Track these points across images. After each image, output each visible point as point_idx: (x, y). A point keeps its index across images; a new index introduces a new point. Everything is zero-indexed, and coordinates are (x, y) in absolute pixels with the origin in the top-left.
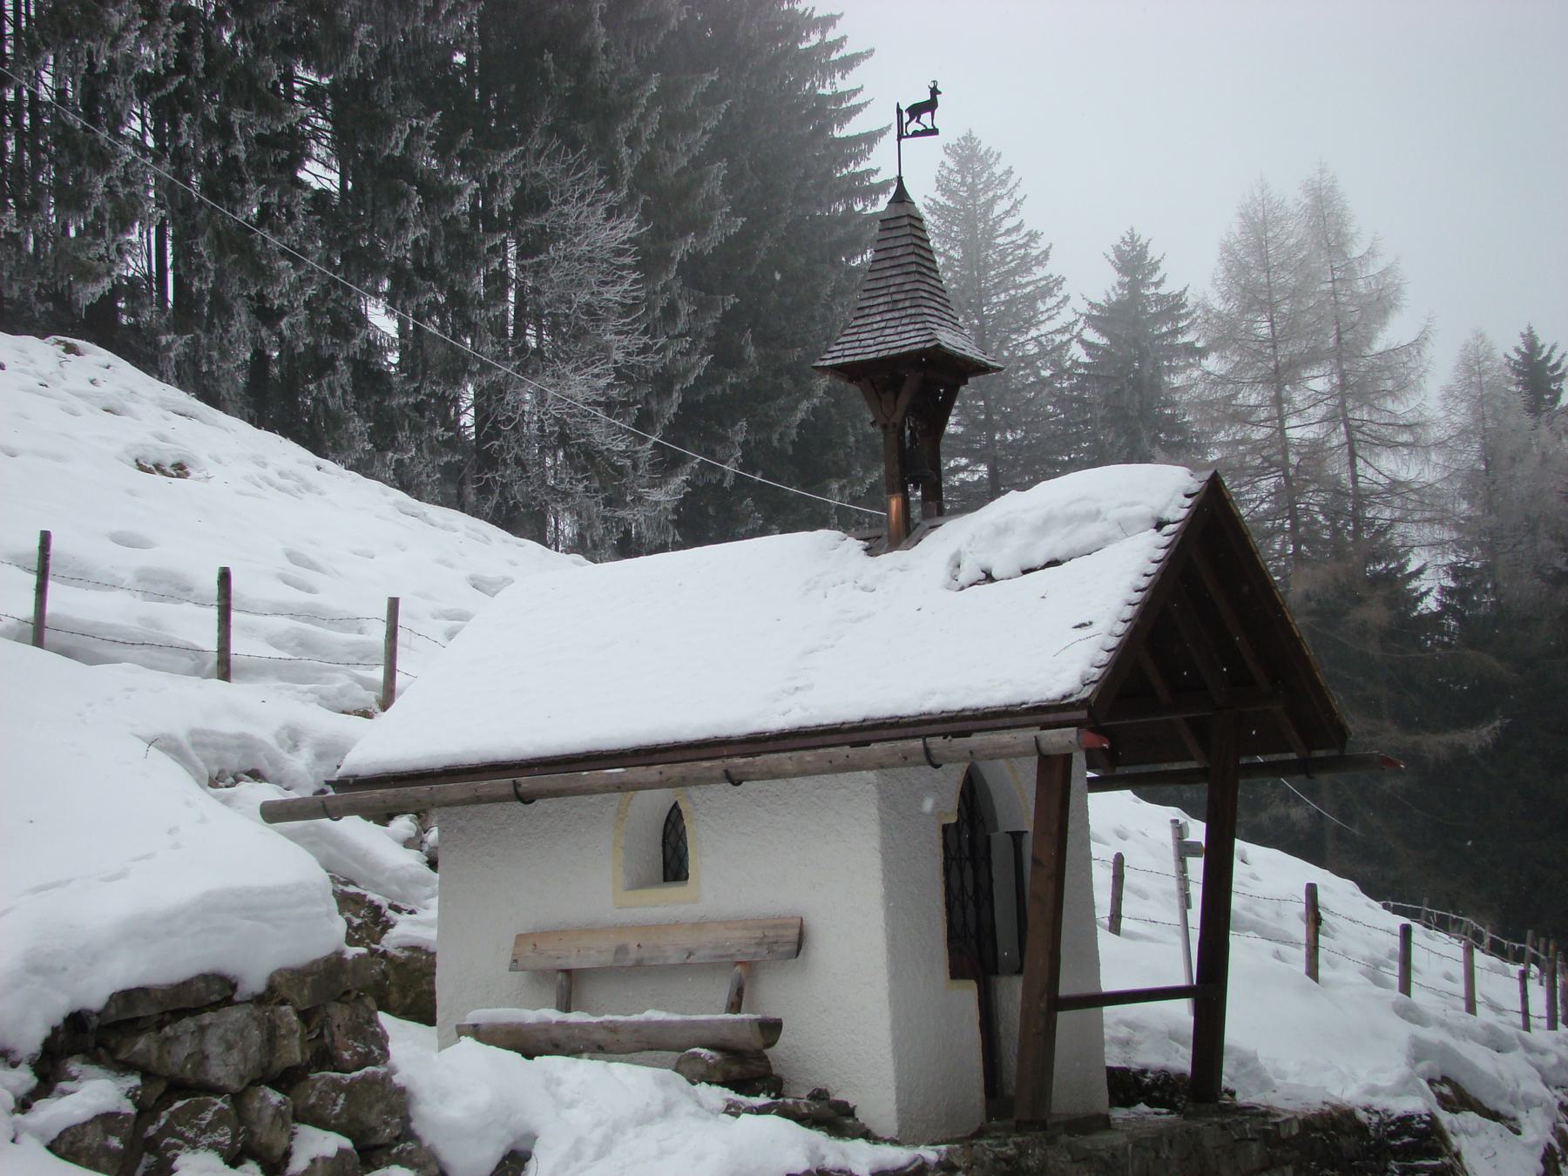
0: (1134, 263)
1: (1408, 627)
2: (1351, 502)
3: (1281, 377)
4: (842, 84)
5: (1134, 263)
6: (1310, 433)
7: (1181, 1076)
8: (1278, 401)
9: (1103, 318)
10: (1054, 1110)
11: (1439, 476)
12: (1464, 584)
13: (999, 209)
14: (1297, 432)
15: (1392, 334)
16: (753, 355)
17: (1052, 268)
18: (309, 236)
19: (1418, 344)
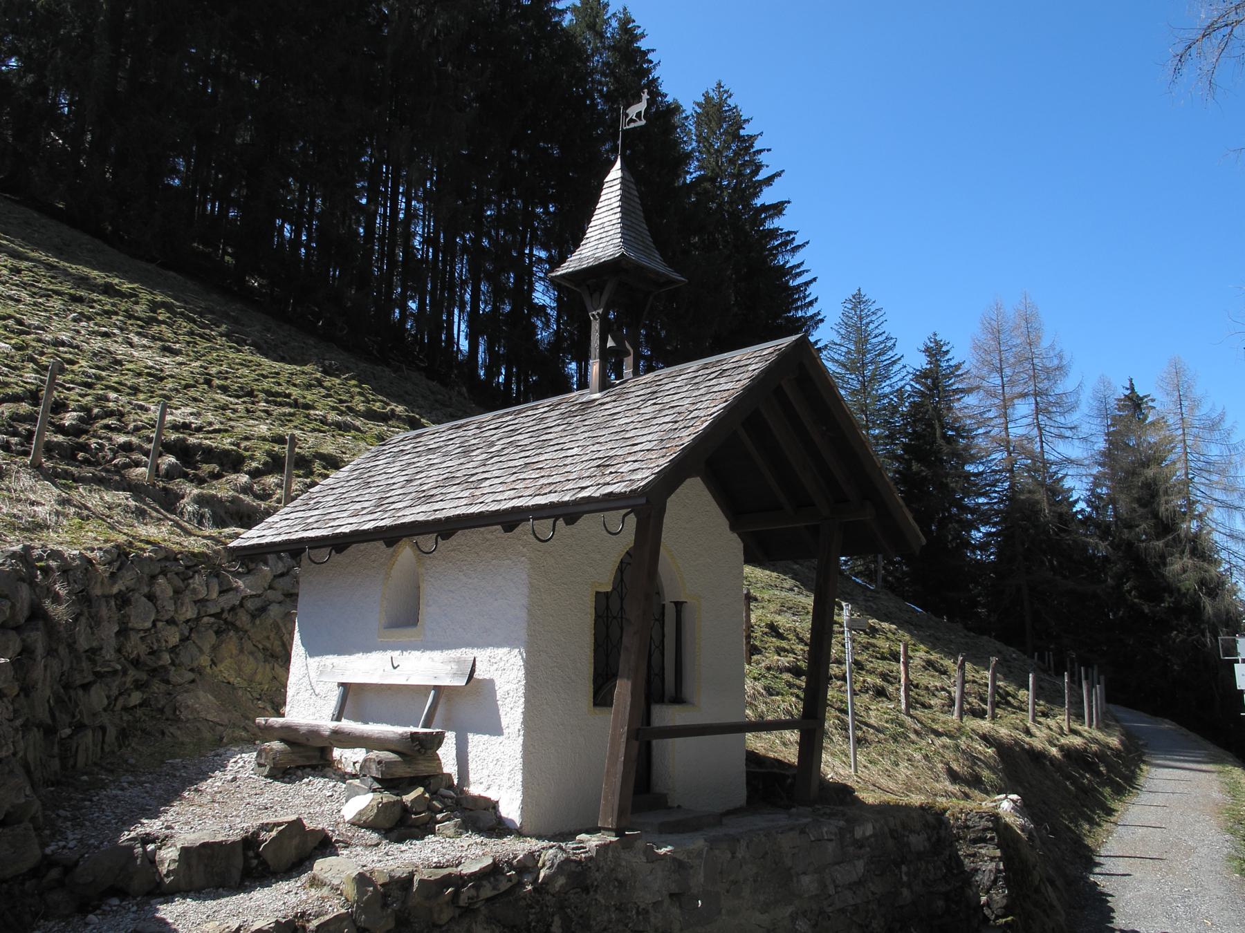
0: (935, 351)
1: (1065, 518)
2: (1040, 465)
3: (1005, 407)
4: (811, 311)
5: (935, 351)
6: (1021, 431)
7: (790, 766)
8: (1005, 415)
9: (921, 376)
10: (630, 683)
11: (1085, 455)
12: (1094, 500)
13: (872, 326)
14: (1016, 431)
15: (1065, 385)
16: (1006, 731)
17: (898, 351)
18: (962, 667)
19: (1076, 392)
